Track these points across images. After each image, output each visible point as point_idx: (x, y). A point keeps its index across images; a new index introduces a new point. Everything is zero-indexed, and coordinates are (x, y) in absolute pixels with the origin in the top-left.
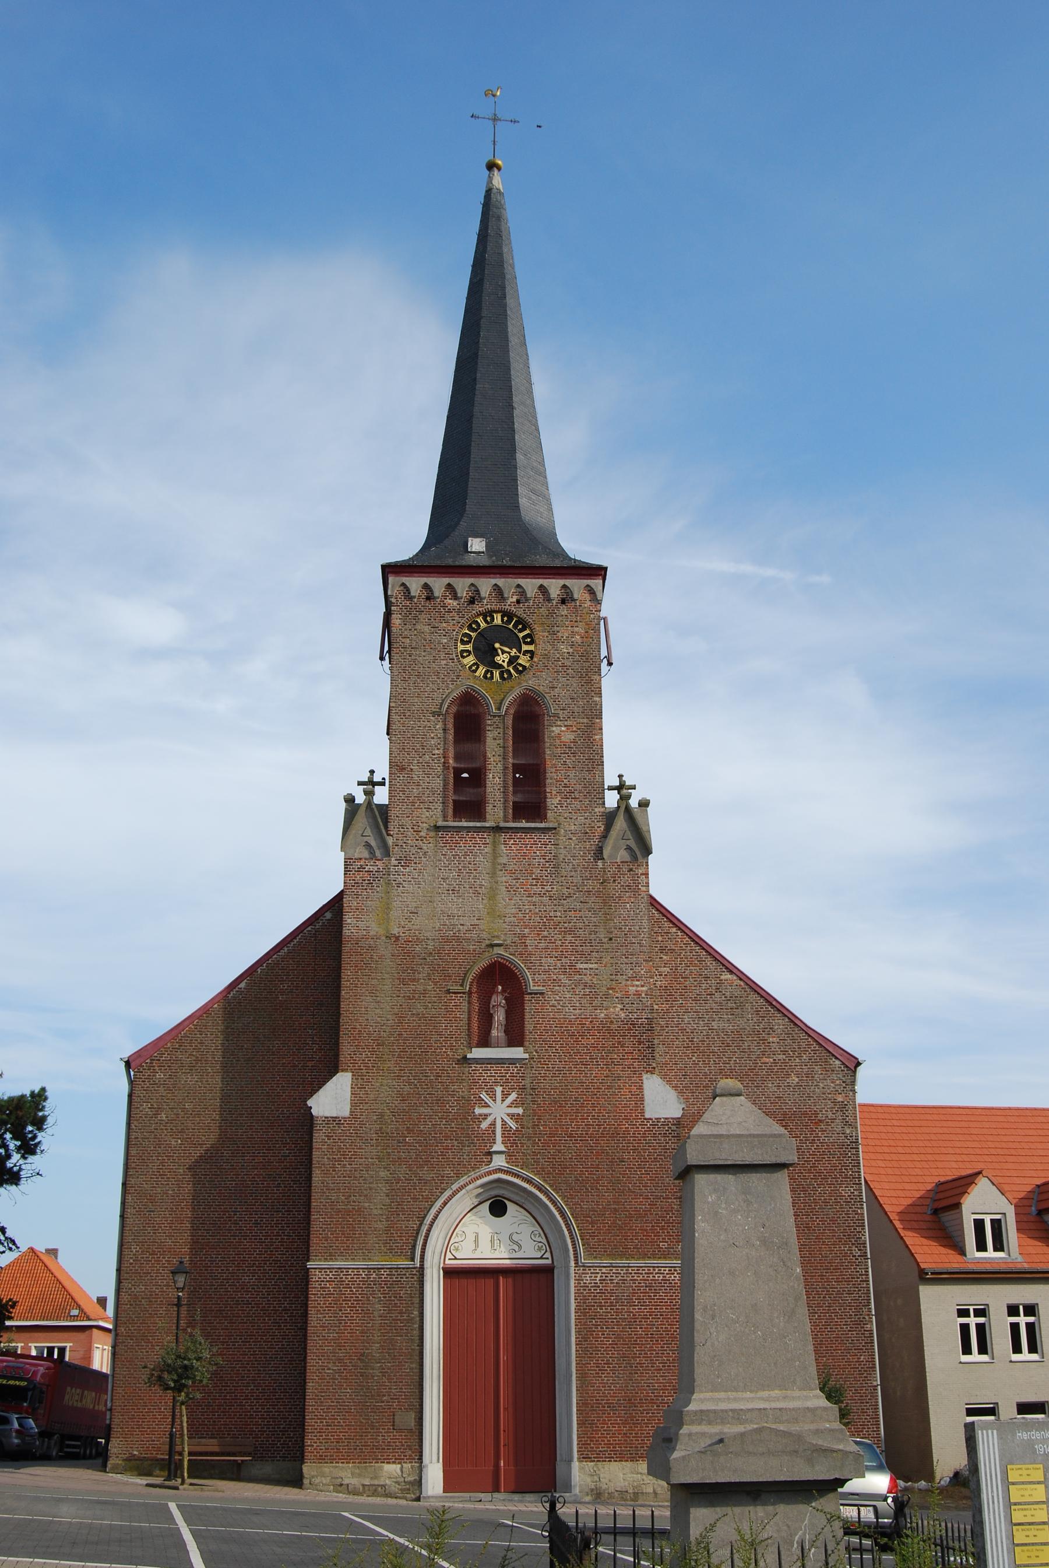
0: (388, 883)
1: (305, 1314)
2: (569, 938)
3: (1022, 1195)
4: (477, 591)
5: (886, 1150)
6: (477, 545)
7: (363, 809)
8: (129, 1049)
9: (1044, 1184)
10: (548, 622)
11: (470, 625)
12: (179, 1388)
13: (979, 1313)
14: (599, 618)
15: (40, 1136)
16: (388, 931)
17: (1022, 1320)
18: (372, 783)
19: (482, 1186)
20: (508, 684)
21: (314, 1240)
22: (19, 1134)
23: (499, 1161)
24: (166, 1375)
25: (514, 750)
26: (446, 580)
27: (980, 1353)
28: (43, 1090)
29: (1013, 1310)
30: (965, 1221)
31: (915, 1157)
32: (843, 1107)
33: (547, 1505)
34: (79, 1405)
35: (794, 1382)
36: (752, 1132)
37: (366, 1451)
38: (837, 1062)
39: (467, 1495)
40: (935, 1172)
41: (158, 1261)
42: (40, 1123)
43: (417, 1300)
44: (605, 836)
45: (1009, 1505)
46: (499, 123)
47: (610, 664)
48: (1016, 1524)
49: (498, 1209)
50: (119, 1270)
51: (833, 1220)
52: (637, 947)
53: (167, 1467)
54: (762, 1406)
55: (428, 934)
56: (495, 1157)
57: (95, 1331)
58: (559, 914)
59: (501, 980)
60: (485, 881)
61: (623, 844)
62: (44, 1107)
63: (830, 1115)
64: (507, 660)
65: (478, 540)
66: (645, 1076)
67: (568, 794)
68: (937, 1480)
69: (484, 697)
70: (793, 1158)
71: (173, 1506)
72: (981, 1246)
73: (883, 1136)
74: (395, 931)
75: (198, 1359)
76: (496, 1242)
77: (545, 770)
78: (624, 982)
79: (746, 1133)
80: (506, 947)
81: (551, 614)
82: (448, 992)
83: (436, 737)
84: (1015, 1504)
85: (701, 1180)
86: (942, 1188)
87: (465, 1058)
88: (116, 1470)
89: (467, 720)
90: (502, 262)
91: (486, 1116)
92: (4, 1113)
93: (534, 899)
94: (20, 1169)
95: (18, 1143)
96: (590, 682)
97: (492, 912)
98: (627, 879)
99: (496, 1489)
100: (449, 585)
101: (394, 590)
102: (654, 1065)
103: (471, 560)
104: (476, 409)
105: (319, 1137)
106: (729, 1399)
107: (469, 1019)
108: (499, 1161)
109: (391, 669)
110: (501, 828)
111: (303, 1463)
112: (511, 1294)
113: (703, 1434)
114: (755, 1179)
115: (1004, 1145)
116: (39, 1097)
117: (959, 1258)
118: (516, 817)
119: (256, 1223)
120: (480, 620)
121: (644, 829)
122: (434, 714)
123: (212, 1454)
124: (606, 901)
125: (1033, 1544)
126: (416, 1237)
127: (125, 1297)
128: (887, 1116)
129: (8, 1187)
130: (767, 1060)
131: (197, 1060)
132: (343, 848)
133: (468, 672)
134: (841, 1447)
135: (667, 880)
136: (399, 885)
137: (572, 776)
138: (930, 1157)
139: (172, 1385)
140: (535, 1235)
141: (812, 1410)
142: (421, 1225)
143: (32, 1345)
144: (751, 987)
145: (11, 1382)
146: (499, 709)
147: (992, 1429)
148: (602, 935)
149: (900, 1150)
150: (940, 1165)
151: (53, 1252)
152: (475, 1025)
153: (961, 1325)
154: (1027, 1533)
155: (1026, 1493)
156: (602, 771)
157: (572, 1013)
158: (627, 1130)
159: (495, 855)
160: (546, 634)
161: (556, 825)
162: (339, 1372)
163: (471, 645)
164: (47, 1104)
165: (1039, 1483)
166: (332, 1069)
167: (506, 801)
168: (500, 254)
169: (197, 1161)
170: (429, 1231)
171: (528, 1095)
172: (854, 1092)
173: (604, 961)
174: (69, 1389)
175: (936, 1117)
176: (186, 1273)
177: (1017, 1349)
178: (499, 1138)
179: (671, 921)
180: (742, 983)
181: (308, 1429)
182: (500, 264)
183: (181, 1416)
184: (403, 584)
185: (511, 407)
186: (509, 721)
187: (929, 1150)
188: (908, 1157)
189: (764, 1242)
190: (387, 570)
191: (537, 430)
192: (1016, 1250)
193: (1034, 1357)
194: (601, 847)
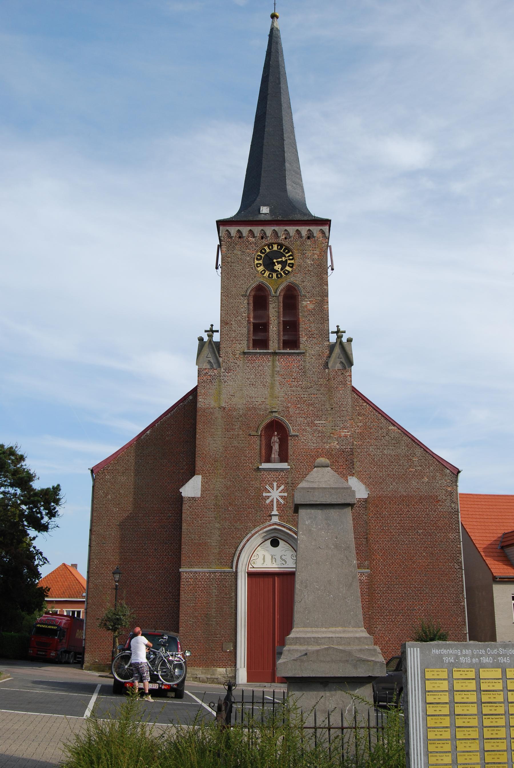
0: (220, 381)
1: (179, 595)
2: (311, 408)
4: (265, 233)
5: (478, 517)
6: (265, 210)
7: (207, 344)
10: (301, 248)
11: (261, 251)
15: (57, 508)
16: (219, 404)
20: (280, 280)
21: (183, 558)
22: (47, 507)
23: (275, 519)
24: (108, 623)
25: (283, 314)
26: (249, 228)
28: (59, 485)
32: (451, 494)
33: (227, 687)
36: (332, 486)
38: (448, 471)
39: (259, 684)
40: (502, 528)
42: (57, 501)
43: (233, 588)
44: (329, 357)
45: (425, 692)
47: (332, 269)
48: (428, 704)
49: (275, 543)
52: (345, 412)
54: (330, 636)
55: (240, 406)
56: (273, 517)
58: (306, 396)
59: (276, 428)
60: (269, 380)
61: (338, 360)
62: (59, 494)
64: (280, 268)
65: (266, 207)
66: (349, 477)
67: (311, 336)
75: (124, 615)
76: (274, 562)
78: (339, 430)
79: (329, 486)
81: (302, 244)
82: (250, 435)
83: (244, 306)
84: (429, 691)
86: (506, 536)
87: (258, 468)
89: (260, 299)
90: (279, 65)
91: (268, 497)
92: (40, 496)
93: (293, 388)
94: (48, 524)
95: (47, 511)
96: (322, 279)
97: (272, 396)
98: (340, 378)
100: (250, 230)
102: (354, 472)
103: (261, 218)
105: (185, 507)
106: (313, 631)
107: (260, 448)
108: (275, 519)
110: (277, 353)
114: (333, 513)
116: (57, 489)
118: (284, 347)
120: (266, 248)
121: (349, 353)
122: (243, 296)
125: (439, 715)
126: (234, 557)
128: (479, 500)
129: (43, 533)
130: (412, 470)
131: (126, 469)
132: (197, 364)
134: (373, 659)
135: (362, 378)
137: (312, 326)
138: (500, 521)
139: (111, 628)
140: (293, 556)
141: (359, 639)
142: (236, 551)
143: (65, 610)
144: (404, 433)
145: (49, 627)
146: (276, 293)
147: (417, 647)
148: (328, 406)
150: (505, 524)
151: (75, 566)
152: (263, 451)
154: (435, 709)
155: (436, 685)
157: (312, 446)
159: (274, 366)
160: (300, 254)
161: (304, 351)
162: (195, 623)
163: (262, 261)
164: (60, 492)
165: (444, 679)
166: (192, 473)
167: (279, 339)
168: (278, 61)
170: (240, 554)
172: (457, 486)
173: (329, 420)
174: (78, 630)
176: (120, 573)
179: (363, 400)
180: (399, 431)
184: (227, 230)
185: (283, 140)
186: (281, 299)
189: (336, 547)
190: (219, 223)
194: (327, 362)
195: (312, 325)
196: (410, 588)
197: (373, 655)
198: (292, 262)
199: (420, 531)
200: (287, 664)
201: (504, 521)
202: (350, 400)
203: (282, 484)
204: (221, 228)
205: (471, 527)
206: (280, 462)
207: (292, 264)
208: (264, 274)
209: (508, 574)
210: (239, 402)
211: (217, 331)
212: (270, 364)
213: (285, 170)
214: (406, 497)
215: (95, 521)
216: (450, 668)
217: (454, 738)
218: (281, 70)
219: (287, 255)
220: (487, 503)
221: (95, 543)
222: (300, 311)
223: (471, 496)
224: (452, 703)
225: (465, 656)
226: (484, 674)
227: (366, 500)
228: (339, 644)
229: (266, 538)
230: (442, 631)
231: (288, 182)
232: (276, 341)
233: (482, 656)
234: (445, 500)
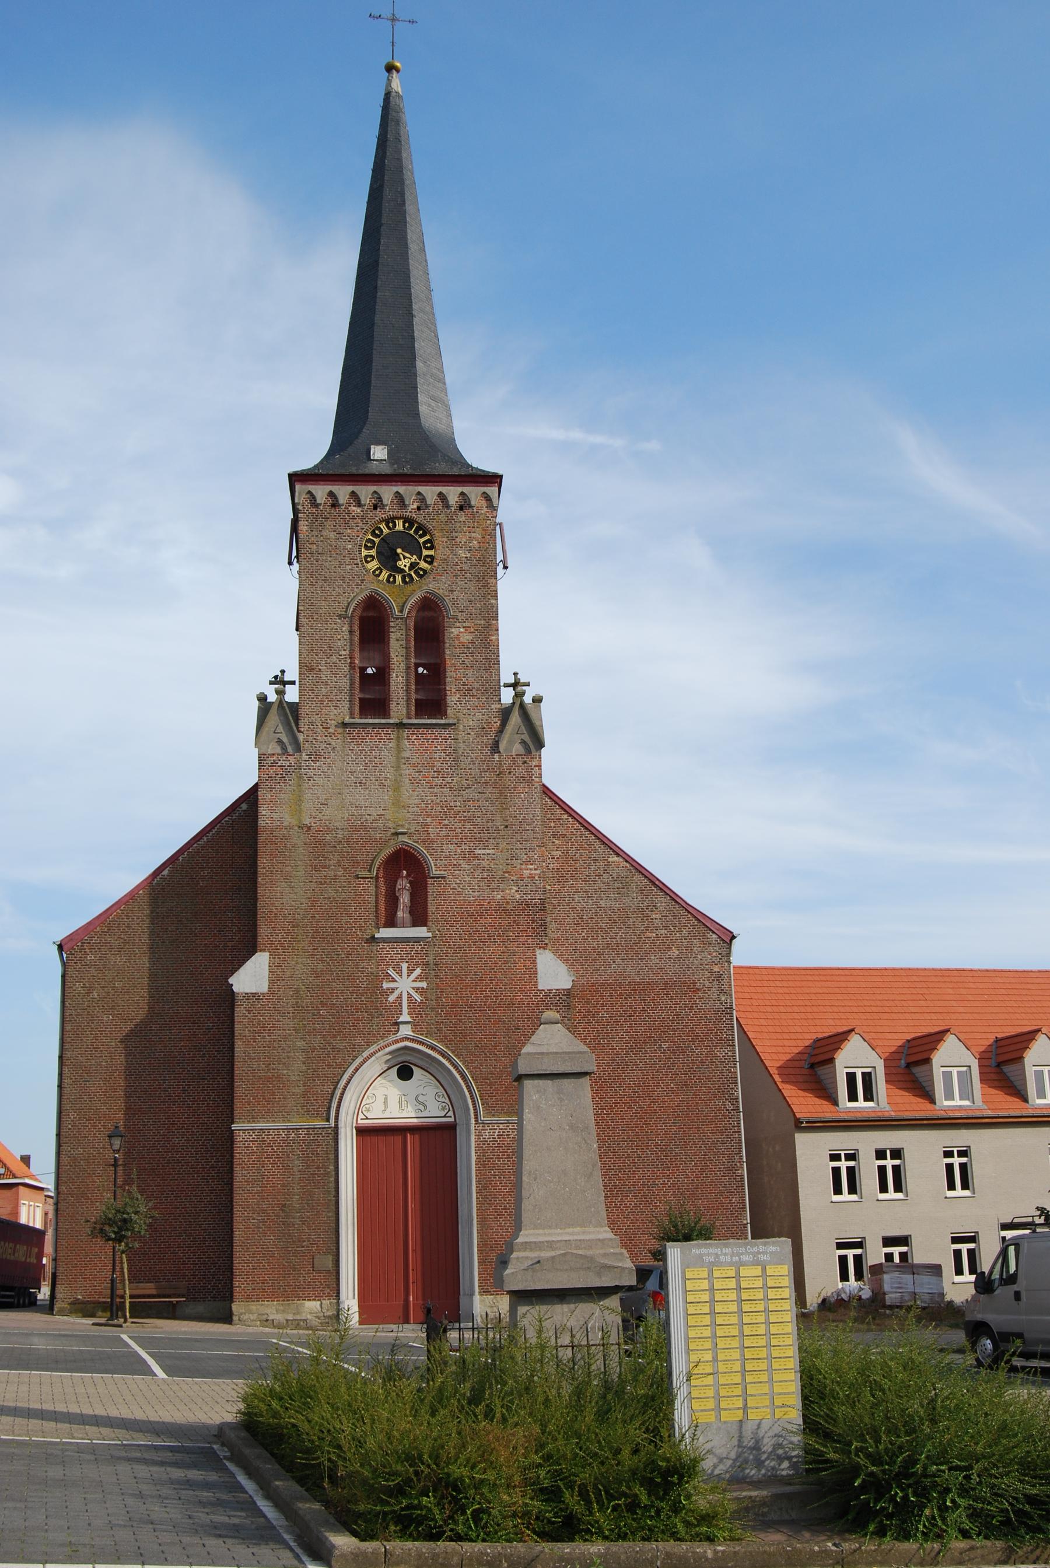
0: (300, 777)
1: (231, 1171)
3: (893, 1049)
4: (380, 498)
5: (769, 1009)
6: (379, 452)
8: (62, 933)
9: (914, 1039)
10: (447, 528)
11: (374, 531)
12: (119, 1239)
13: (850, 1157)
14: (496, 524)
16: (300, 821)
17: (889, 1163)
19: (390, 1053)
20: (409, 588)
21: (237, 1104)
23: (406, 1031)
24: (107, 1228)
26: (350, 488)
27: (895, 1191)
29: (880, 1154)
30: (838, 1075)
31: (796, 1016)
32: (719, 977)
34: (12, 1258)
35: (590, 1222)
37: (290, 1291)
38: (714, 936)
41: (95, 1127)
43: (332, 1157)
44: (501, 731)
45: (686, 1292)
46: (397, 23)
47: (505, 568)
50: (58, 1135)
51: (709, 1079)
53: (111, 1309)
54: (567, 1238)
55: (337, 824)
56: (401, 1026)
57: (21, 1188)
58: (458, 804)
59: (405, 865)
61: (518, 738)
63: (707, 984)
66: (538, 952)
67: (467, 692)
68: (808, 1304)
70: (595, 1069)
71: (125, 1337)
72: (853, 1097)
73: (767, 996)
74: (307, 821)
75: (136, 1213)
77: (445, 669)
81: (450, 520)
83: (342, 636)
85: (528, 1084)
86: (819, 1044)
87: (373, 937)
88: (62, 1313)
89: (372, 625)
96: (486, 585)
97: (397, 803)
98: (521, 771)
99: (407, 1322)
101: (301, 498)
103: (373, 468)
104: (377, 319)
107: (377, 902)
109: (299, 572)
111: (232, 1301)
112: (418, 1149)
113: (527, 1258)
114: (566, 1083)
115: (879, 1003)
117: (833, 1108)
118: (418, 715)
119: (184, 1090)
120: (383, 526)
121: (537, 723)
122: (340, 616)
123: (149, 1296)
124: (502, 792)
126: (331, 1100)
127: (65, 1159)
131: (125, 942)
133: (370, 577)
135: (561, 768)
137: (470, 675)
138: (809, 1016)
141: (1008, 1267)
142: (335, 1089)
146: (401, 611)
149: (782, 1009)
150: (818, 1022)
152: (382, 907)
153: (879, 1167)
156: (498, 670)
157: (471, 895)
158: (522, 1001)
159: (399, 749)
160: (445, 539)
166: (250, 949)
167: (408, 699)
168: (400, 160)
169: (127, 1035)
170: (342, 1094)
171: (431, 970)
173: (501, 847)
175: (816, 978)
177: (884, 1189)
181: (236, 1272)
182: (399, 169)
183: (122, 1263)
184: (309, 492)
185: (411, 315)
187: (809, 1009)
188: (789, 1016)
189: (572, 1127)
191: (437, 336)
192: (885, 1100)
193: (967, 1193)
195: (470, 672)
196: (647, 1147)
197: (621, 1260)
199: (665, 1046)
201: (816, 1016)
202: (538, 812)
204: (298, 487)
205: (757, 1029)
206: (414, 926)
207: (431, 557)
208: (379, 575)
209: (822, 1115)
210: (336, 816)
211: (293, 683)
214: (639, 984)
215: (69, 1040)
216: (711, 1267)
217: (714, 1336)
218: (405, 177)
220: (785, 984)
222: (447, 645)
223: (757, 971)
224: (712, 1302)
225: (725, 1255)
226: (744, 1272)
227: (568, 993)
228: (578, 1247)
230: (703, 1221)
231: (421, 398)
232: (403, 702)
233: (742, 1254)
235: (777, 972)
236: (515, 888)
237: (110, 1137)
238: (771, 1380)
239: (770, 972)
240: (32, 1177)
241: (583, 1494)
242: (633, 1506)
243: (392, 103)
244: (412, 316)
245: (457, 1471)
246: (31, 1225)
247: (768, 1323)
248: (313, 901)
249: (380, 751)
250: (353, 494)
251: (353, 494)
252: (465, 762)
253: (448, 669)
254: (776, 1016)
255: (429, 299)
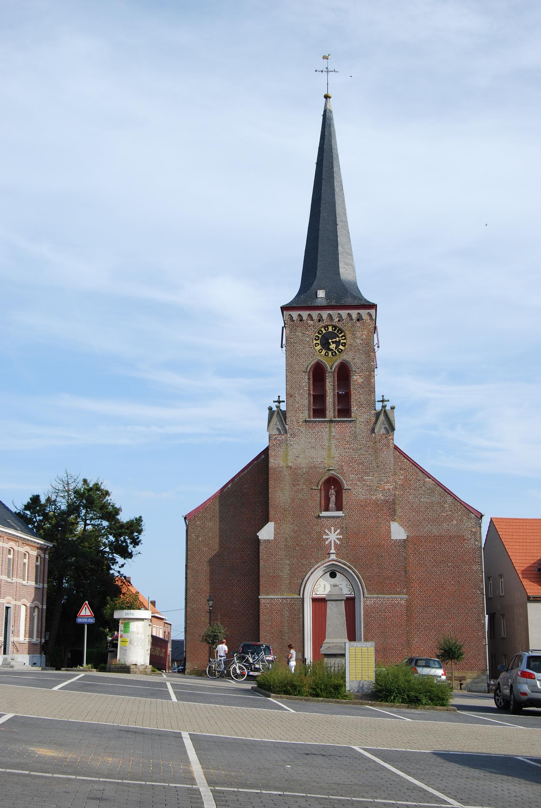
0: (287, 445)
1: (259, 616)
2: (361, 466)
5: (521, 541)
6: (321, 294)
7: (276, 413)
16: (287, 464)
18: (279, 402)
19: (325, 567)
20: (335, 358)
21: (261, 587)
23: (333, 557)
24: (208, 638)
26: (308, 312)
28: (141, 517)
31: (535, 544)
32: (475, 534)
38: (473, 515)
41: (201, 595)
42: (140, 532)
43: (301, 610)
44: (376, 423)
49: (333, 575)
50: (186, 599)
51: (469, 579)
55: (303, 466)
56: (331, 555)
59: (333, 484)
60: (326, 443)
61: (383, 426)
66: (391, 523)
67: (361, 406)
69: (325, 364)
73: (521, 534)
74: (290, 464)
75: (220, 633)
80: (335, 470)
81: (353, 326)
82: (312, 489)
83: (305, 381)
89: (318, 373)
90: (332, 149)
97: (329, 456)
98: (385, 441)
101: (287, 318)
104: (321, 226)
107: (320, 500)
114: (338, 602)
116: (139, 520)
120: (323, 329)
121: (391, 419)
122: (304, 372)
124: (376, 451)
128: (524, 524)
131: (213, 516)
133: (317, 354)
136: (291, 445)
146: (331, 369)
148: (374, 465)
152: (323, 502)
156: (375, 395)
158: (384, 544)
159: (330, 432)
164: (143, 523)
166: (266, 520)
167: (334, 410)
168: (331, 145)
170: (306, 584)
171: (344, 530)
173: (375, 475)
178: (333, 547)
184: (290, 315)
188: (531, 544)
189: (339, 613)
191: (348, 232)
196: (441, 609)
198: (345, 341)
200: (324, 650)
202: (392, 460)
203: (338, 528)
204: (285, 312)
205: (514, 551)
207: (345, 343)
208: (321, 352)
210: (303, 463)
211: (284, 402)
212: (327, 430)
213: (338, 254)
214: (438, 536)
219: (340, 336)
220: (531, 528)
221: (190, 576)
222: (352, 384)
223: (518, 521)
227: (405, 541)
229: (326, 571)
231: (341, 265)
232: (332, 411)
234: (470, 539)
235: (528, 521)
236: (381, 494)
237: (208, 600)
238: (368, 672)
239: (525, 521)
240: (157, 613)
241: (321, 689)
242: (330, 692)
243: (327, 116)
244: (336, 225)
245: (295, 683)
246: (158, 636)
247: (368, 660)
248: (293, 500)
249: (322, 433)
250: (309, 315)
251: (309, 315)
252: (359, 438)
253: (352, 395)
254: (525, 544)
255: (345, 214)
